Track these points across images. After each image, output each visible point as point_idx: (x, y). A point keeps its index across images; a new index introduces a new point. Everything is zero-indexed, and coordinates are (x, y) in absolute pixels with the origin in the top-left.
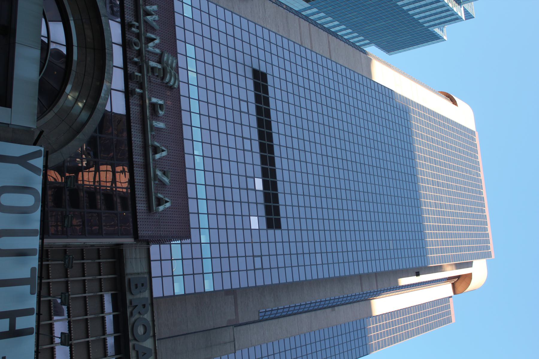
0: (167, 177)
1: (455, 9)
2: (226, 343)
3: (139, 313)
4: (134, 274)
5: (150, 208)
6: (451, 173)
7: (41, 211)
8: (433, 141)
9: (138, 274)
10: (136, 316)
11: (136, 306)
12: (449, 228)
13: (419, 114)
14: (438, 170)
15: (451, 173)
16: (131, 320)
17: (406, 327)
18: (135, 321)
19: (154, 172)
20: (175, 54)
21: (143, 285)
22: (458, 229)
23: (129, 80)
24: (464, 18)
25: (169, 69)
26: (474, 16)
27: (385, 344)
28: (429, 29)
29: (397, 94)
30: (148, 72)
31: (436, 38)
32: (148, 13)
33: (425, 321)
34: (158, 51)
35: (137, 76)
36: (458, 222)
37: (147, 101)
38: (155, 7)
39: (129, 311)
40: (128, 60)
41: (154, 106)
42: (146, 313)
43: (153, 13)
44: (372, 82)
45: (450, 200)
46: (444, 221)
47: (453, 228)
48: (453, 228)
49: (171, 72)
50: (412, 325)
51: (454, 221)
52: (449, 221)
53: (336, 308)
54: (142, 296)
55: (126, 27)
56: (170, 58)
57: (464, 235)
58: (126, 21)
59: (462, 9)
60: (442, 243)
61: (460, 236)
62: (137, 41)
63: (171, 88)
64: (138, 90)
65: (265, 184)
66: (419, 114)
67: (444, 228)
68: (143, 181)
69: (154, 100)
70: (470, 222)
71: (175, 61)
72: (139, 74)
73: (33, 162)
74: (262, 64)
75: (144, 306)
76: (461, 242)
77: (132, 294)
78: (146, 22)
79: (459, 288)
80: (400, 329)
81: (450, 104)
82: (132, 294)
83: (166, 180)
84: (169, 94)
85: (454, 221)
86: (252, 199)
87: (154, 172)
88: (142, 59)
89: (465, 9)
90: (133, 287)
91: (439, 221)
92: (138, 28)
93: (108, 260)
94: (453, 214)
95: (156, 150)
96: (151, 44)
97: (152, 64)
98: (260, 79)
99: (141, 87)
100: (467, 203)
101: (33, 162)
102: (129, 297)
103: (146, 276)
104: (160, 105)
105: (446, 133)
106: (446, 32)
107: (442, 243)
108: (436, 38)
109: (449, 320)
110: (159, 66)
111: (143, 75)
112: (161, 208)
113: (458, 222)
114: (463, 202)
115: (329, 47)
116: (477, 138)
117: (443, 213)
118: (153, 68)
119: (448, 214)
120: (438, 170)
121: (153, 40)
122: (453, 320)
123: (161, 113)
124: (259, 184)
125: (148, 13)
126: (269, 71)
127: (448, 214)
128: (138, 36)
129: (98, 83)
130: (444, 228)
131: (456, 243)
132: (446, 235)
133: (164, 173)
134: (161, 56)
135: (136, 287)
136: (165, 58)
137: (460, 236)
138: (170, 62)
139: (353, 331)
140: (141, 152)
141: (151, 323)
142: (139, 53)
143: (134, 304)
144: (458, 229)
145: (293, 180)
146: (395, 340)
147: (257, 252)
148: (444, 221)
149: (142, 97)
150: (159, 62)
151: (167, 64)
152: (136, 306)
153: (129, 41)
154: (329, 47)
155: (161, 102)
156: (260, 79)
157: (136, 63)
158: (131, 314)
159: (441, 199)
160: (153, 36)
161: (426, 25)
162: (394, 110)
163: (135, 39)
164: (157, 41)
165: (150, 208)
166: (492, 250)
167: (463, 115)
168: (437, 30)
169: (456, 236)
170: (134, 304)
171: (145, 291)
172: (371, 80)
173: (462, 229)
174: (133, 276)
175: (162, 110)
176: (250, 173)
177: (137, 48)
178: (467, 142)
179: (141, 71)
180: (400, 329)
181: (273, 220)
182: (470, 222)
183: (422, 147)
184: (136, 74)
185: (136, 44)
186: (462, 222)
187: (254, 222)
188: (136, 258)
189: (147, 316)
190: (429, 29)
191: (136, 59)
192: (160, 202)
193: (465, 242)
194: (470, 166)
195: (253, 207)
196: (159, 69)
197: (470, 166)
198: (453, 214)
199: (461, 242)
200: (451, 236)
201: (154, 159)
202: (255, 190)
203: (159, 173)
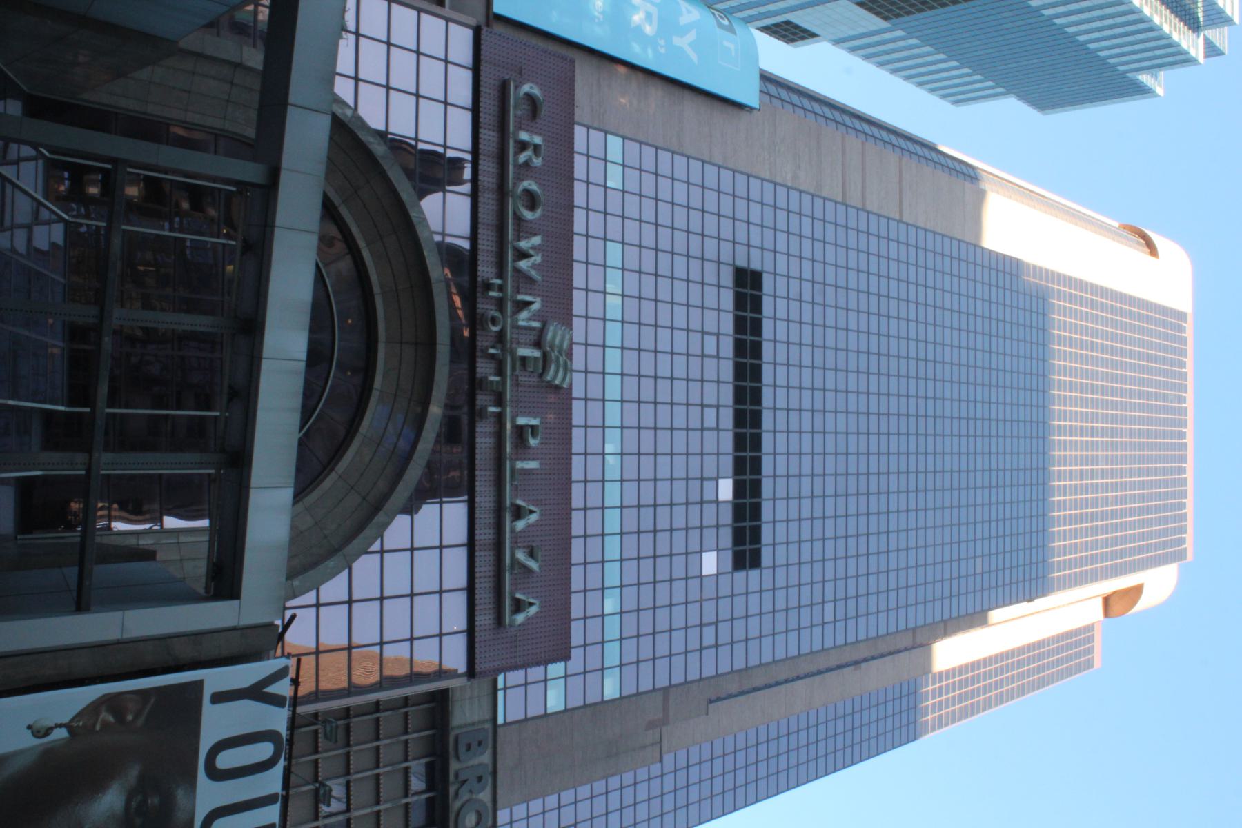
0: (536, 560)
1: (1184, 45)
2: (644, 747)
3: (471, 791)
4: (466, 726)
5: (499, 620)
6: (1124, 406)
7: (285, 768)
8: (1092, 347)
9: (473, 724)
10: (465, 796)
11: (465, 781)
12: (1103, 515)
13: (1072, 298)
14: (1096, 404)
15: (1124, 406)
16: (455, 805)
17: (997, 685)
18: (462, 806)
19: (513, 555)
20: (566, 318)
21: (480, 743)
22: (1123, 513)
23: (478, 392)
24: (1201, 59)
25: (553, 355)
26: (1226, 52)
27: (953, 718)
28: (1129, 75)
29: (1028, 265)
30: (513, 369)
31: (1142, 91)
32: (523, 255)
33: (1040, 669)
34: (536, 324)
35: (492, 382)
36: (1124, 500)
37: (509, 426)
38: (536, 240)
39: (452, 790)
40: (478, 354)
41: (520, 431)
42: (483, 789)
43: (532, 252)
44: (979, 251)
45: (1114, 460)
46: (1095, 502)
47: (1113, 514)
48: (1113, 514)
49: (558, 358)
50: (1012, 679)
51: (1116, 501)
52: (1106, 501)
53: (864, 665)
54: (476, 761)
55: (479, 290)
56: (560, 332)
57: (1133, 525)
58: (479, 279)
59: (1201, 41)
60: (1086, 547)
61: (1124, 526)
62: (497, 314)
63: (558, 388)
64: (492, 409)
65: (739, 489)
66: (1072, 298)
67: (1094, 517)
68: (488, 574)
69: (521, 421)
70: (1151, 497)
71: (567, 337)
72: (497, 379)
73: (271, 689)
74: (755, 253)
75: (480, 779)
76: (1124, 540)
77: (458, 758)
78: (517, 271)
79: (1115, 607)
80: (986, 689)
81: (1142, 256)
82: (458, 758)
83: (533, 565)
84: (552, 400)
85: (1116, 501)
86: (710, 519)
87: (513, 555)
88: (504, 350)
89: (1206, 40)
90: (462, 749)
91: (1085, 503)
92: (501, 288)
93: (423, 734)
94: (1115, 487)
95: (518, 513)
96: (524, 315)
97: (523, 352)
98: (748, 284)
99: (500, 400)
100: (1150, 459)
101: (271, 689)
102: (454, 766)
103: (488, 726)
104: (532, 427)
105: (1124, 326)
106: (1159, 82)
107: (1086, 547)
108: (1142, 91)
109: (1089, 665)
110: (537, 353)
111: (504, 383)
112: (520, 618)
113: (1124, 500)
114: (1141, 459)
115: (900, 182)
116: (1189, 326)
117: (1096, 488)
118: (524, 359)
119: (1105, 488)
120: (1096, 404)
121: (528, 304)
122: (1097, 663)
123: (533, 442)
124: (726, 490)
125: (523, 255)
126: (768, 267)
127: (1105, 488)
128: (500, 304)
129: (419, 409)
130: (1094, 517)
131: (1115, 542)
132: (1096, 531)
133: (531, 555)
134: (542, 332)
135: (469, 747)
136: (549, 336)
137: (1124, 526)
138: (557, 341)
139: (934, 564)
140: (492, 521)
141: (489, 805)
142: (500, 338)
143: (462, 778)
144: (1123, 513)
145: (842, 283)
146: (974, 710)
147: (709, 617)
148: (1095, 502)
149: (500, 418)
150: (538, 344)
151: (552, 347)
152: (465, 781)
153: (483, 315)
154: (900, 182)
155: (534, 422)
156: (748, 284)
157: (493, 356)
158: (457, 794)
159: (1095, 461)
160: (528, 298)
161: (1121, 68)
162: (1017, 302)
163: (494, 312)
164: (535, 307)
165: (499, 620)
166: (1189, 545)
167: (1165, 279)
168: (1145, 78)
169: (1115, 528)
170: (462, 778)
171: (482, 754)
172: (977, 246)
173: (1132, 512)
174: (464, 730)
175: (534, 435)
176: (710, 471)
177: (495, 329)
178: (1167, 337)
179: (500, 371)
180: (986, 689)
181: (746, 552)
182: (1151, 497)
183: (1067, 364)
184: (492, 378)
185: (494, 321)
186: (1134, 499)
187: (710, 563)
188: (471, 698)
189: (485, 796)
190: (1129, 75)
191: (492, 351)
192: (518, 606)
193: (1133, 538)
194: (1166, 386)
195: (710, 535)
196: (536, 358)
197: (1166, 386)
198: (1115, 487)
199: (1124, 540)
200: (1105, 530)
201: (513, 531)
202: (717, 502)
203: (521, 556)
